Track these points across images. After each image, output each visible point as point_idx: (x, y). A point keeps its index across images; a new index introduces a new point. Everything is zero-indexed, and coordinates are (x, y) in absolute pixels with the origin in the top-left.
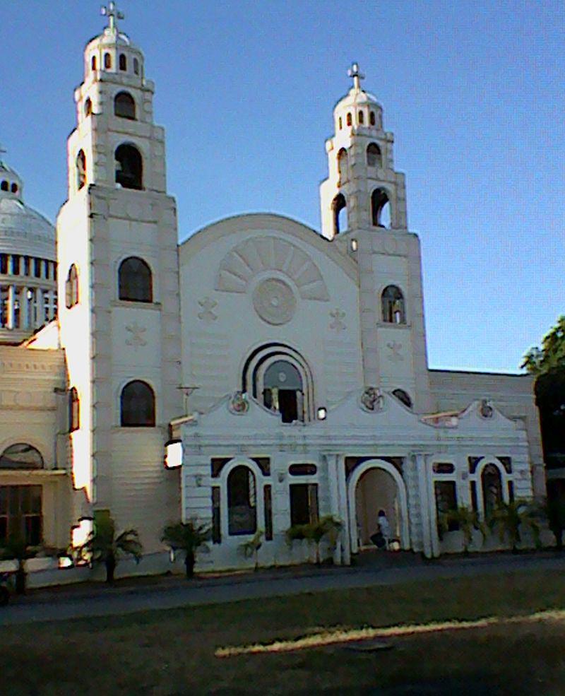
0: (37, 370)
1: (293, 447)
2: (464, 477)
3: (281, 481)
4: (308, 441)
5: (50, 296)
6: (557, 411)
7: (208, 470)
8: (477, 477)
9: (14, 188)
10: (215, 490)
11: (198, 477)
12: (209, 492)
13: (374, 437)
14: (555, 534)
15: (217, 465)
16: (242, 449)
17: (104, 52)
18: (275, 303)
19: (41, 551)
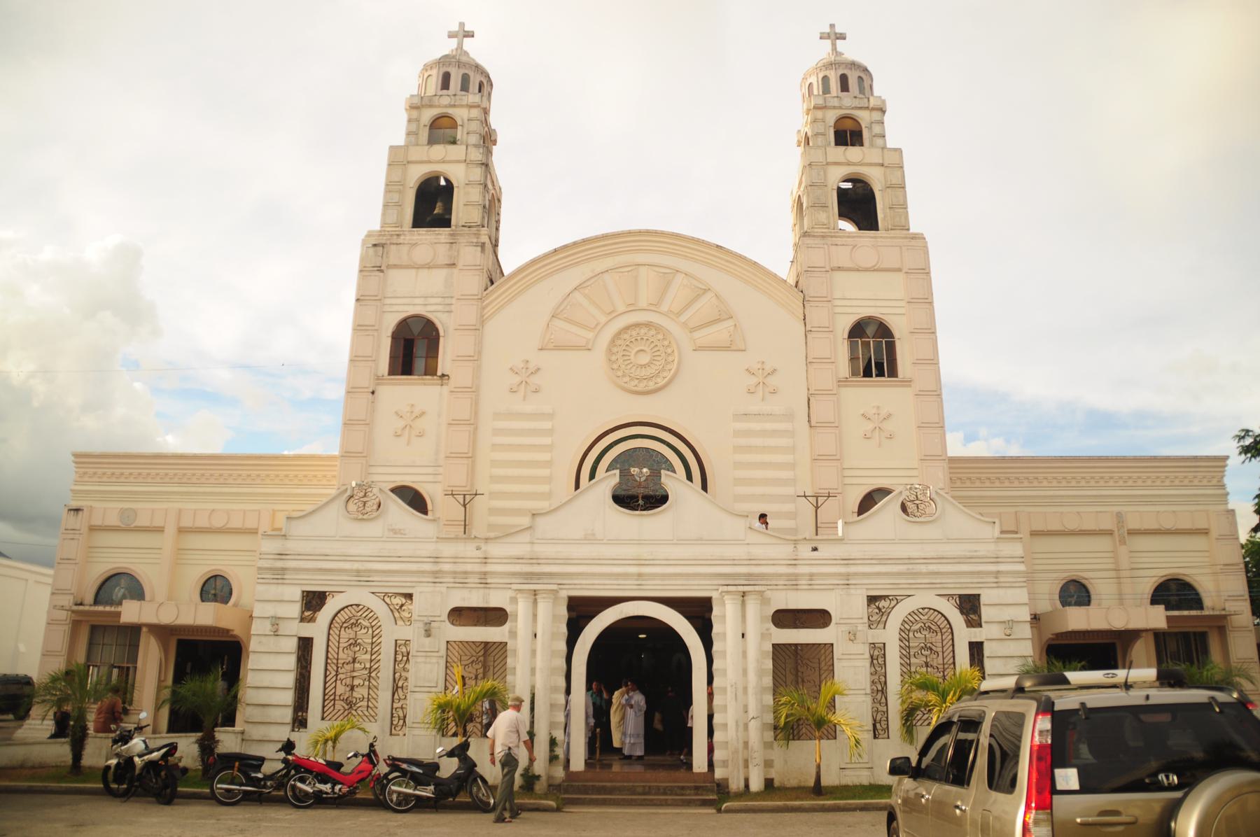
0: (767, 532)
1: (461, 579)
2: (852, 636)
3: (428, 633)
4: (489, 568)
5: (1140, 483)
6: (637, 469)
7: (295, 610)
8: (890, 635)
9: (709, 289)
10: (305, 645)
11: (276, 621)
12: (292, 645)
13: (640, 562)
14: (595, 723)
15: (313, 601)
16: (361, 577)
17: (821, 76)
18: (644, 359)
19: (919, 761)
